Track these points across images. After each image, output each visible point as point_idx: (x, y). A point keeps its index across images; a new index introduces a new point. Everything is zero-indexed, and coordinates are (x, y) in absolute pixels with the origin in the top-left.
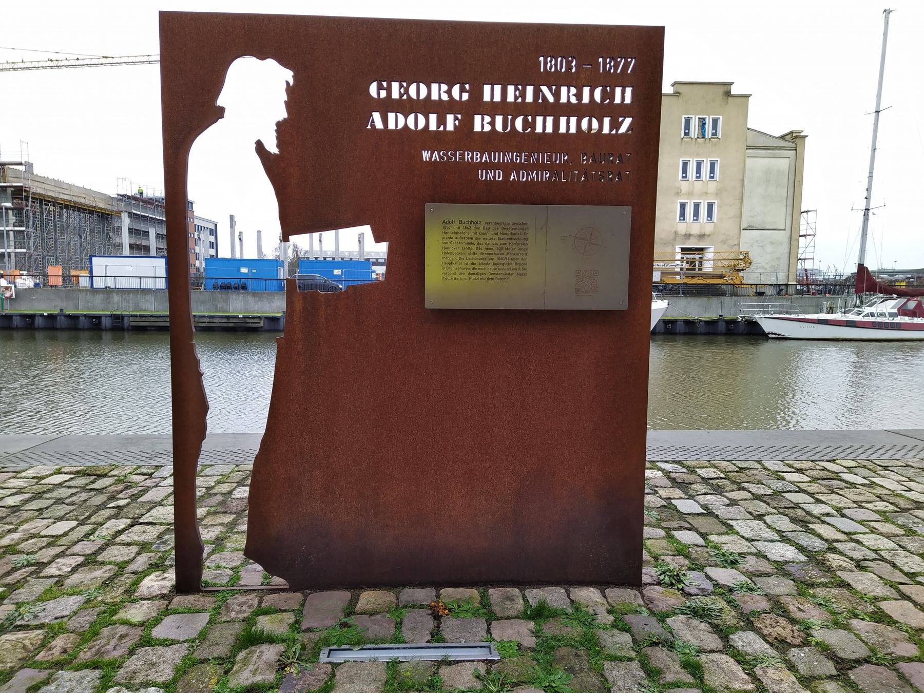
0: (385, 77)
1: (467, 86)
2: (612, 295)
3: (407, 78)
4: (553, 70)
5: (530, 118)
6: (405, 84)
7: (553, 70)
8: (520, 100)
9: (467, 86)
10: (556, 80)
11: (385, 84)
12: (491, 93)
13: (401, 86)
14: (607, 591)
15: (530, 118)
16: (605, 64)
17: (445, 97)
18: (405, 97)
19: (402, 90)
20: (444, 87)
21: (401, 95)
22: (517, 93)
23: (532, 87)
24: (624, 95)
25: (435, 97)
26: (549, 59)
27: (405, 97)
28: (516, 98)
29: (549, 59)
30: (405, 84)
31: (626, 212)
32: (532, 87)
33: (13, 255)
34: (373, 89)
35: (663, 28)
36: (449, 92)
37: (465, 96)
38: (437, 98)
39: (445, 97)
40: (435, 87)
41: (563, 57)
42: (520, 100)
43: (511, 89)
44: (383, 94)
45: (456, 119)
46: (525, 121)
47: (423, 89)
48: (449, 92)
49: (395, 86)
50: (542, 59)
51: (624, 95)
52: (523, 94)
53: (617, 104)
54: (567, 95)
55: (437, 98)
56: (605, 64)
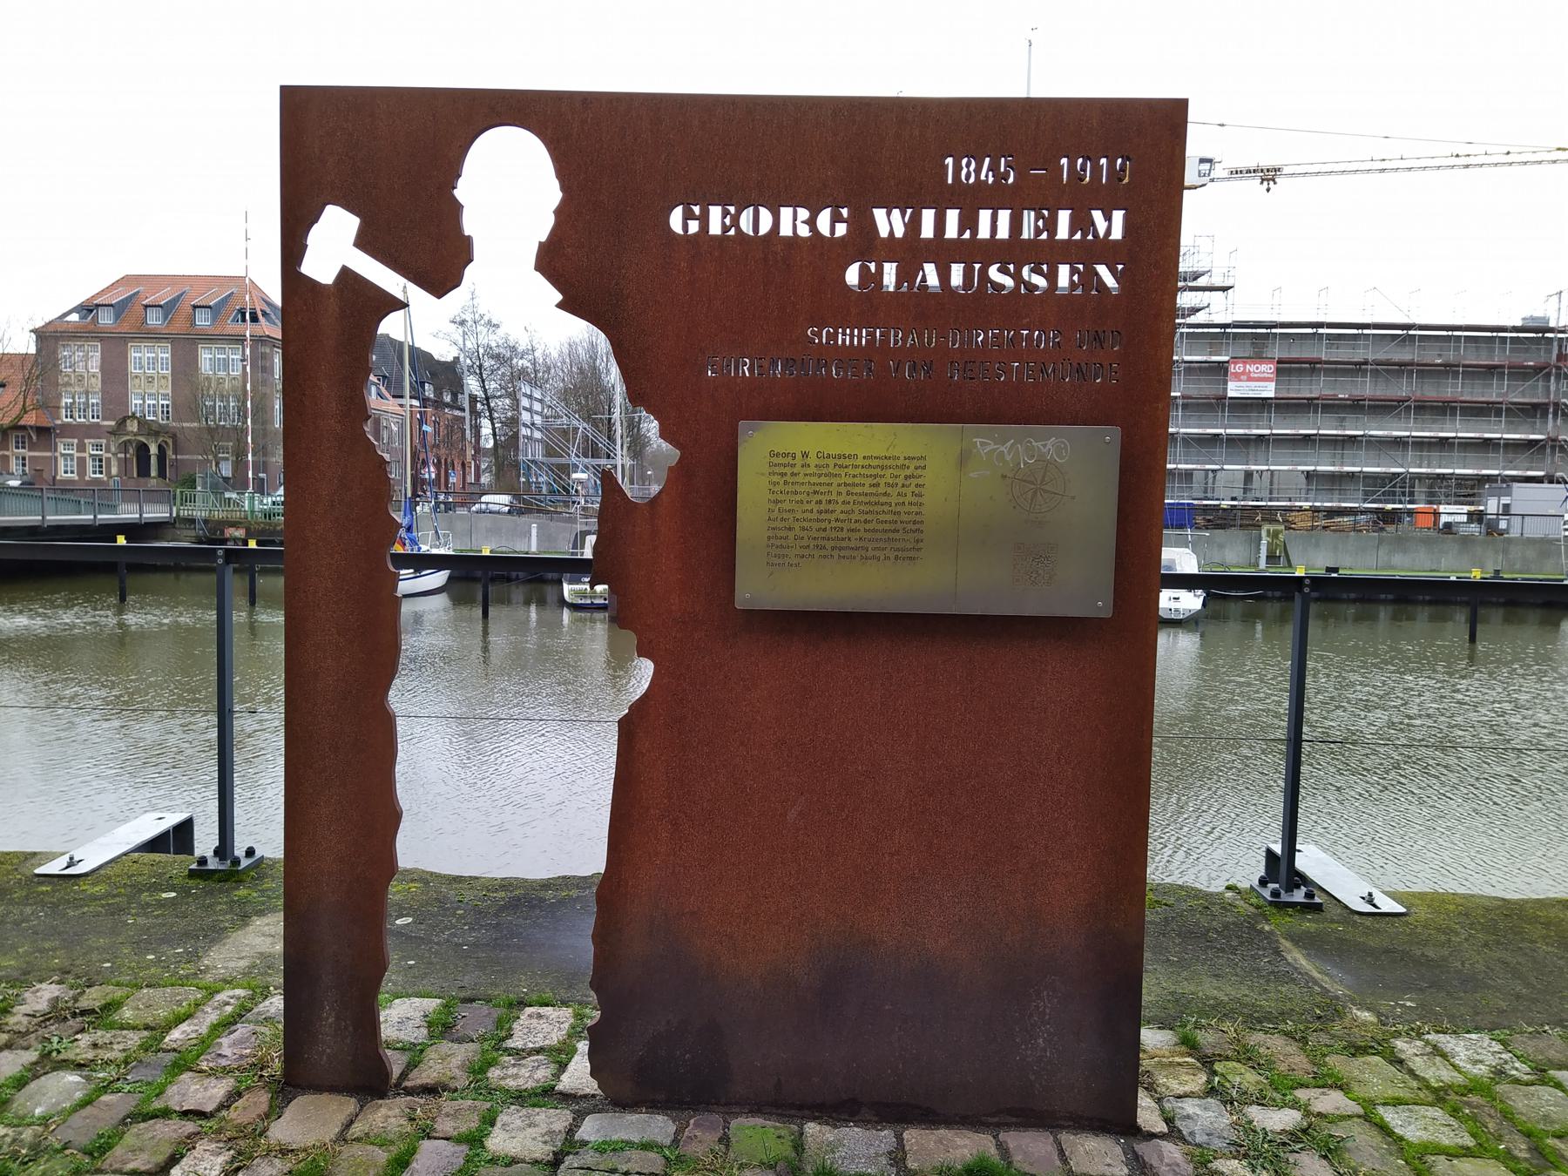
0: (698, 196)
1: (845, 212)
2: (1081, 588)
3: (738, 197)
4: (972, 180)
5: (872, 266)
6: (732, 209)
7: (972, 180)
8: (1044, 236)
9: (845, 212)
10: (971, 200)
11: (697, 210)
12: (889, 223)
13: (725, 213)
14: (1002, 1136)
15: (872, 266)
16: (957, 169)
17: (804, 231)
18: (732, 232)
19: (728, 221)
20: (803, 214)
21: (725, 229)
22: (1040, 223)
23: (933, 211)
24: (1113, 225)
25: (786, 230)
26: (965, 161)
27: (732, 232)
28: (1038, 232)
29: (965, 161)
30: (732, 209)
31: (1110, 436)
32: (933, 211)
33: (1266, 476)
34: (676, 219)
35: (282, 88)
36: (811, 223)
37: (841, 230)
38: (790, 234)
39: (804, 231)
40: (786, 213)
41: (1086, 158)
42: (1044, 236)
43: (1029, 217)
44: (694, 227)
45: (1073, 271)
46: (864, 271)
47: (766, 218)
48: (811, 223)
49: (715, 212)
50: (949, 161)
51: (1113, 225)
52: (1051, 226)
53: (1062, 241)
54: (994, 224)
55: (790, 234)
56: (957, 169)
